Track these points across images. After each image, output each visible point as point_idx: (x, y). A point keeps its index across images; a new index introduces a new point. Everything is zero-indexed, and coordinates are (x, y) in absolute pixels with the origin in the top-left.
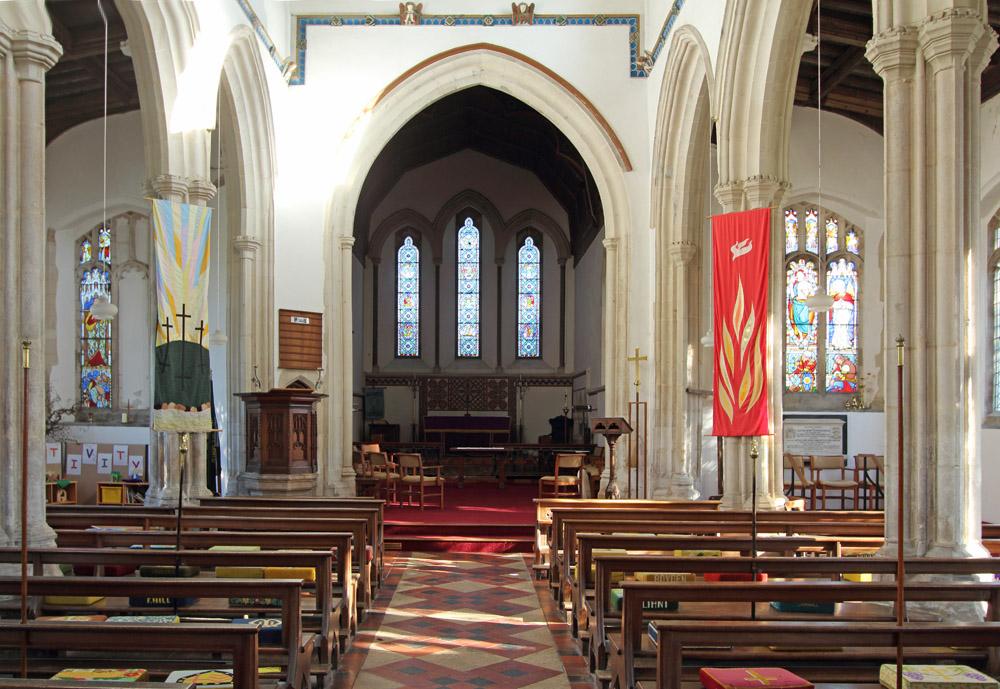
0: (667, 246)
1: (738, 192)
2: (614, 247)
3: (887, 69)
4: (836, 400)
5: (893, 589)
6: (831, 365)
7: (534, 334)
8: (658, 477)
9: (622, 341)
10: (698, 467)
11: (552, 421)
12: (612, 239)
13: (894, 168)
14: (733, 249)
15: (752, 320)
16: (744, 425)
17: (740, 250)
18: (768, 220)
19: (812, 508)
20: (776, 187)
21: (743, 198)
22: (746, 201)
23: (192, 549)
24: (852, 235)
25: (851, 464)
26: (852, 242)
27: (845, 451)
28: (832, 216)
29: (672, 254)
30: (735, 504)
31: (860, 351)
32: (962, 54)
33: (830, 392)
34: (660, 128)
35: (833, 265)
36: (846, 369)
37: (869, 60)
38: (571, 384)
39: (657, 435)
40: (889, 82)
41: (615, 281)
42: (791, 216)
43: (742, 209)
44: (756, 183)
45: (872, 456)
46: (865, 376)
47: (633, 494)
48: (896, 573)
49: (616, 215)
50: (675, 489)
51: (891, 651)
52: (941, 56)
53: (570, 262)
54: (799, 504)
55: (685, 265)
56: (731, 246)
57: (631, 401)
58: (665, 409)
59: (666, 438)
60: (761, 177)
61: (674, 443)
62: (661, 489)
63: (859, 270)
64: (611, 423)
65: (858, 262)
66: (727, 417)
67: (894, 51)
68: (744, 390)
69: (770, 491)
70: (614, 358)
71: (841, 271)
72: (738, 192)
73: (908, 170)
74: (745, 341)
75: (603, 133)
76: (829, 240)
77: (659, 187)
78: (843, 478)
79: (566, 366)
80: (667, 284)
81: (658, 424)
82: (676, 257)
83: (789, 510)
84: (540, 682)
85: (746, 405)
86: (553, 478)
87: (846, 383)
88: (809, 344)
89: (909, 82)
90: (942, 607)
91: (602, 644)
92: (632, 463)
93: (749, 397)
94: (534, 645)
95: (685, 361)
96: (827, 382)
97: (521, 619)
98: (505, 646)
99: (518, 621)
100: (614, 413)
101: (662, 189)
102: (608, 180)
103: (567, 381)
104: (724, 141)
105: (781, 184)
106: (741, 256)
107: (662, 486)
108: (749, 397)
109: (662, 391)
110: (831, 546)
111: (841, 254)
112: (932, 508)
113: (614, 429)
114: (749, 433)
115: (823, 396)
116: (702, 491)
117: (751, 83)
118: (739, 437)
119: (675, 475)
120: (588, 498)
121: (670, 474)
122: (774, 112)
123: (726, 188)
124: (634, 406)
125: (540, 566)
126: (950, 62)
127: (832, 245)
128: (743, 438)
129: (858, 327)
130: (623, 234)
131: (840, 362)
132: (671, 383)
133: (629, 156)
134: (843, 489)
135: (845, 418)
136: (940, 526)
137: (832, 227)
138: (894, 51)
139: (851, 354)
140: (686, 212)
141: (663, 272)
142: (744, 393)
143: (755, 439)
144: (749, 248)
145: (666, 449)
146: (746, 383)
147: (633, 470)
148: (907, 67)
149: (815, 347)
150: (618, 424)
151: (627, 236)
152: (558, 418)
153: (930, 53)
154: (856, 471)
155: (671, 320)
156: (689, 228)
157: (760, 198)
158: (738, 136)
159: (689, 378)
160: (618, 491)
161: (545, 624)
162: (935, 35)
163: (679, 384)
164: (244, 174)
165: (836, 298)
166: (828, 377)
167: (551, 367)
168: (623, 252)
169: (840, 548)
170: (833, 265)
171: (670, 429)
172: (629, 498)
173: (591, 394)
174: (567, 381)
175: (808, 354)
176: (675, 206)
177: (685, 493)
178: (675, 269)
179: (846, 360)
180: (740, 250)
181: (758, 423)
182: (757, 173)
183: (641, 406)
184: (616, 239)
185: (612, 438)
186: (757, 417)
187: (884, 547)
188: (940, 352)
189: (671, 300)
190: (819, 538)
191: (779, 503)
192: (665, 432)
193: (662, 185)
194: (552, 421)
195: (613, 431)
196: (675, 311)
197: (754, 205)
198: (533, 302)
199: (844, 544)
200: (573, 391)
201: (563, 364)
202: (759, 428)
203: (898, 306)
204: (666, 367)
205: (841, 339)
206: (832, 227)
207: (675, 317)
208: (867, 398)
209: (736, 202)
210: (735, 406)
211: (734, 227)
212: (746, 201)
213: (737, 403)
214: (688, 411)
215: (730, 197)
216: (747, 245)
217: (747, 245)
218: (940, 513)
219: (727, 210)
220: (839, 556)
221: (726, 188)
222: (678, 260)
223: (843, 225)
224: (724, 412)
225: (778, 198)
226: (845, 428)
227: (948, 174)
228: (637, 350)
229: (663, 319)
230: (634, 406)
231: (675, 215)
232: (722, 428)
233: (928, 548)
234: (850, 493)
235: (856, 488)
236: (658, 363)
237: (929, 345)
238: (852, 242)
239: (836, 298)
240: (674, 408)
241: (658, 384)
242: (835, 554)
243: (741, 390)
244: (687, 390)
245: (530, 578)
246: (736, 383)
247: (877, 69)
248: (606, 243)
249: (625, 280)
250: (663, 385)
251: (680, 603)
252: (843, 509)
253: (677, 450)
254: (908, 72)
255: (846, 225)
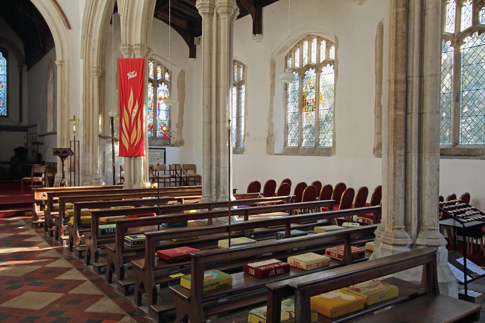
0: (89, 68)
1: (130, 49)
2: (61, 65)
3: (204, 13)
4: (161, 142)
5: (227, 212)
6: (159, 127)
7: (3, 104)
8: (85, 176)
9: (66, 111)
10: (104, 171)
11: (15, 150)
12: (61, 61)
13: (206, 53)
14: (128, 74)
15: (137, 107)
16: (132, 152)
17: (131, 75)
18: (144, 61)
19: (165, 186)
20: (147, 50)
21: (133, 53)
22: (134, 55)
23: (319, 193)
24: (167, 73)
25: (168, 168)
26: (167, 76)
27: (165, 163)
28: (159, 64)
29: (92, 72)
30: (129, 186)
31: (170, 121)
32: (230, 14)
33: (158, 138)
34: (86, 12)
35: (160, 85)
36: (164, 129)
37: (197, 8)
38: (26, 131)
39: (85, 156)
40: (204, 19)
41: (62, 81)
42: (151, 63)
43: (132, 57)
44: (139, 47)
45: (179, 165)
46: (172, 132)
47: (73, 184)
48: (208, 208)
49: (62, 50)
50: (94, 181)
51: (227, 234)
52: (223, 13)
53: (25, 68)
54: (156, 185)
55: (98, 78)
56: (127, 73)
57: (71, 140)
58: (89, 144)
59: (89, 157)
60: (141, 45)
61: (93, 160)
62: (87, 181)
63: (170, 88)
64: (63, 150)
65: (169, 85)
66: (125, 148)
67: (207, 7)
68: (133, 136)
69: (144, 180)
70: (62, 119)
71: (163, 87)
72: (130, 49)
73: (211, 54)
74: (134, 115)
75: (56, 8)
76: (158, 74)
77: (85, 40)
78: (165, 174)
79: (23, 121)
80: (89, 86)
81: (85, 151)
82: (94, 74)
83: (152, 187)
84: (64, 274)
85: (134, 143)
86: (30, 178)
87: (164, 135)
88: (150, 118)
89: (211, 20)
90: (223, 220)
91: (96, 251)
92: (72, 170)
93: (136, 140)
94: (51, 258)
95: (98, 122)
96: (157, 134)
97: (38, 248)
98: (36, 261)
99: (36, 248)
100: (62, 146)
101: (87, 41)
102: (58, 32)
103: (24, 129)
104: (124, 26)
105: (149, 49)
106: (132, 78)
107: (87, 180)
108: (136, 140)
109: (86, 136)
110: (180, 200)
111: (163, 81)
112: (218, 183)
113: (64, 154)
114: (136, 155)
115: (156, 140)
116: (106, 182)
117: (137, 4)
118: (131, 157)
119: (94, 175)
120: (48, 187)
121: (91, 174)
122: (146, 19)
123: (125, 47)
124: (73, 143)
125: (37, 222)
126: (226, 16)
127: (159, 76)
128: (133, 158)
129: (169, 112)
130: (66, 59)
131: (162, 126)
132: (91, 132)
133: (69, 21)
134: (165, 178)
135: (165, 149)
136: (221, 189)
137: (159, 69)
138: (207, 7)
139: (167, 123)
140: (99, 53)
141: (87, 80)
142: (133, 138)
143: (138, 158)
144: (136, 75)
145: (89, 163)
146: (134, 133)
147: (73, 173)
148: (211, 14)
149: (152, 119)
150: (67, 151)
151: (68, 61)
152: (18, 148)
153: (219, 11)
154: (170, 171)
155: (91, 103)
156: (100, 61)
157: (140, 54)
158: (131, 25)
159: (100, 130)
160: (67, 183)
161: (52, 248)
162: (222, 5)
163: (95, 133)
164: (101, 23)
165: (160, 99)
166: (158, 132)
167: (14, 120)
168: (66, 69)
169: (183, 201)
170: (160, 85)
171: (91, 154)
172: (71, 186)
173: (40, 136)
174: (24, 129)
175: (150, 122)
176: (93, 50)
177: (98, 184)
178: (93, 79)
179: (165, 125)
180: (131, 75)
181: (139, 151)
182: (139, 43)
183: (77, 143)
184: (62, 62)
185: (63, 158)
186: (138, 150)
187: (202, 199)
188: (221, 124)
189: (91, 94)
190: (176, 198)
191: (148, 185)
192: (88, 155)
193: (87, 39)
194: (15, 150)
195: (65, 154)
196: (93, 99)
197: (138, 57)
198: (2, 87)
199: (185, 199)
200: (27, 134)
201: (21, 120)
202: (140, 153)
203: (207, 106)
204: (89, 125)
205: (162, 116)
206: (159, 69)
207: (93, 101)
208: (173, 141)
209: (130, 54)
210: (129, 143)
211: (125, 65)
212: (134, 55)
213: (130, 142)
214: (100, 146)
215: (127, 51)
216: (134, 73)
217: (134, 73)
218: (221, 185)
219: (126, 57)
220: (183, 203)
221: (125, 47)
222: (95, 75)
223: (164, 69)
224: (124, 146)
225: (147, 55)
226: (165, 153)
227: (225, 58)
228: (74, 116)
229: (87, 102)
230: (73, 143)
231: (93, 54)
232: (123, 152)
233: (217, 198)
234: (167, 180)
235: (170, 178)
236: (85, 123)
237: (217, 122)
238: (167, 76)
239: (160, 99)
240: (93, 145)
241: (85, 133)
242: (182, 203)
243: (132, 136)
244: (99, 136)
245: (31, 228)
246: (130, 134)
247: (200, 12)
248: (57, 63)
249: (67, 82)
250: (87, 133)
251: (129, 229)
252: (176, 186)
253: (95, 163)
254: (211, 16)
255: (165, 69)
